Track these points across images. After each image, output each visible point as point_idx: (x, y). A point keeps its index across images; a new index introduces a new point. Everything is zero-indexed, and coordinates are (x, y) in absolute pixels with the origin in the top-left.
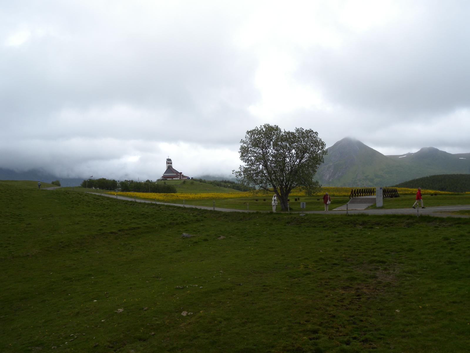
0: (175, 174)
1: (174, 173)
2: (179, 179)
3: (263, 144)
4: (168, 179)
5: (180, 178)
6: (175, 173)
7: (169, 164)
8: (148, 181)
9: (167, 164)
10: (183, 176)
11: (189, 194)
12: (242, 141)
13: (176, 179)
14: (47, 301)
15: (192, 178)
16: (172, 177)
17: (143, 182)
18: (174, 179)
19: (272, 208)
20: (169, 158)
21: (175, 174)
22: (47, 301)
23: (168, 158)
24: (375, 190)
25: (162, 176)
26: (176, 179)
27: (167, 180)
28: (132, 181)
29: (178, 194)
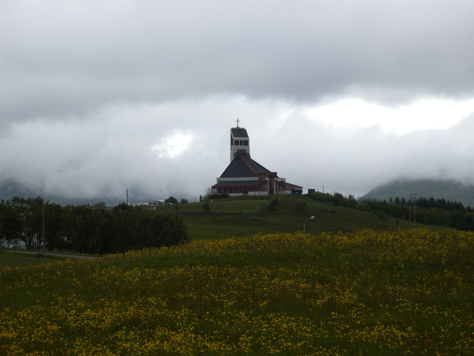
0: (256, 179)
1: (253, 175)
2: (266, 193)
3: (50, 310)
4: (231, 195)
5: (271, 192)
6: (256, 176)
7: (240, 147)
8: (172, 200)
9: (232, 144)
10: (282, 184)
11: (85, 312)
12: (353, 196)
13: (257, 193)
14: (253, 239)
15: (311, 191)
16: (245, 188)
17: (147, 204)
18: (251, 193)
19: (290, 190)
20: (241, 126)
21: (256, 179)
22: (253, 239)
23: (235, 126)
24: (188, 201)
25: (215, 183)
26: (257, 193)
27: (228, 196)
28: (39, 201)
29: (194, 244)
